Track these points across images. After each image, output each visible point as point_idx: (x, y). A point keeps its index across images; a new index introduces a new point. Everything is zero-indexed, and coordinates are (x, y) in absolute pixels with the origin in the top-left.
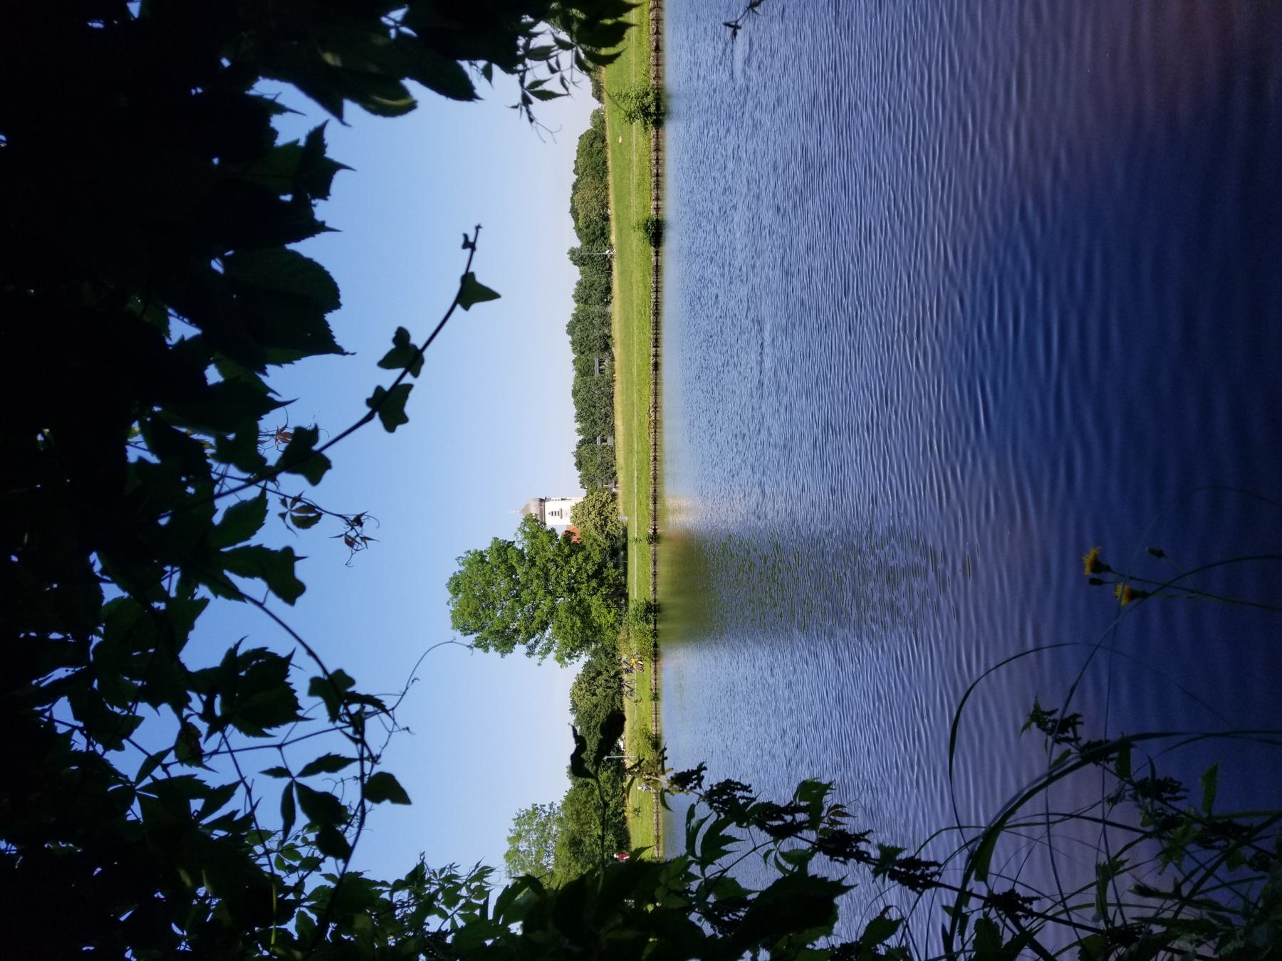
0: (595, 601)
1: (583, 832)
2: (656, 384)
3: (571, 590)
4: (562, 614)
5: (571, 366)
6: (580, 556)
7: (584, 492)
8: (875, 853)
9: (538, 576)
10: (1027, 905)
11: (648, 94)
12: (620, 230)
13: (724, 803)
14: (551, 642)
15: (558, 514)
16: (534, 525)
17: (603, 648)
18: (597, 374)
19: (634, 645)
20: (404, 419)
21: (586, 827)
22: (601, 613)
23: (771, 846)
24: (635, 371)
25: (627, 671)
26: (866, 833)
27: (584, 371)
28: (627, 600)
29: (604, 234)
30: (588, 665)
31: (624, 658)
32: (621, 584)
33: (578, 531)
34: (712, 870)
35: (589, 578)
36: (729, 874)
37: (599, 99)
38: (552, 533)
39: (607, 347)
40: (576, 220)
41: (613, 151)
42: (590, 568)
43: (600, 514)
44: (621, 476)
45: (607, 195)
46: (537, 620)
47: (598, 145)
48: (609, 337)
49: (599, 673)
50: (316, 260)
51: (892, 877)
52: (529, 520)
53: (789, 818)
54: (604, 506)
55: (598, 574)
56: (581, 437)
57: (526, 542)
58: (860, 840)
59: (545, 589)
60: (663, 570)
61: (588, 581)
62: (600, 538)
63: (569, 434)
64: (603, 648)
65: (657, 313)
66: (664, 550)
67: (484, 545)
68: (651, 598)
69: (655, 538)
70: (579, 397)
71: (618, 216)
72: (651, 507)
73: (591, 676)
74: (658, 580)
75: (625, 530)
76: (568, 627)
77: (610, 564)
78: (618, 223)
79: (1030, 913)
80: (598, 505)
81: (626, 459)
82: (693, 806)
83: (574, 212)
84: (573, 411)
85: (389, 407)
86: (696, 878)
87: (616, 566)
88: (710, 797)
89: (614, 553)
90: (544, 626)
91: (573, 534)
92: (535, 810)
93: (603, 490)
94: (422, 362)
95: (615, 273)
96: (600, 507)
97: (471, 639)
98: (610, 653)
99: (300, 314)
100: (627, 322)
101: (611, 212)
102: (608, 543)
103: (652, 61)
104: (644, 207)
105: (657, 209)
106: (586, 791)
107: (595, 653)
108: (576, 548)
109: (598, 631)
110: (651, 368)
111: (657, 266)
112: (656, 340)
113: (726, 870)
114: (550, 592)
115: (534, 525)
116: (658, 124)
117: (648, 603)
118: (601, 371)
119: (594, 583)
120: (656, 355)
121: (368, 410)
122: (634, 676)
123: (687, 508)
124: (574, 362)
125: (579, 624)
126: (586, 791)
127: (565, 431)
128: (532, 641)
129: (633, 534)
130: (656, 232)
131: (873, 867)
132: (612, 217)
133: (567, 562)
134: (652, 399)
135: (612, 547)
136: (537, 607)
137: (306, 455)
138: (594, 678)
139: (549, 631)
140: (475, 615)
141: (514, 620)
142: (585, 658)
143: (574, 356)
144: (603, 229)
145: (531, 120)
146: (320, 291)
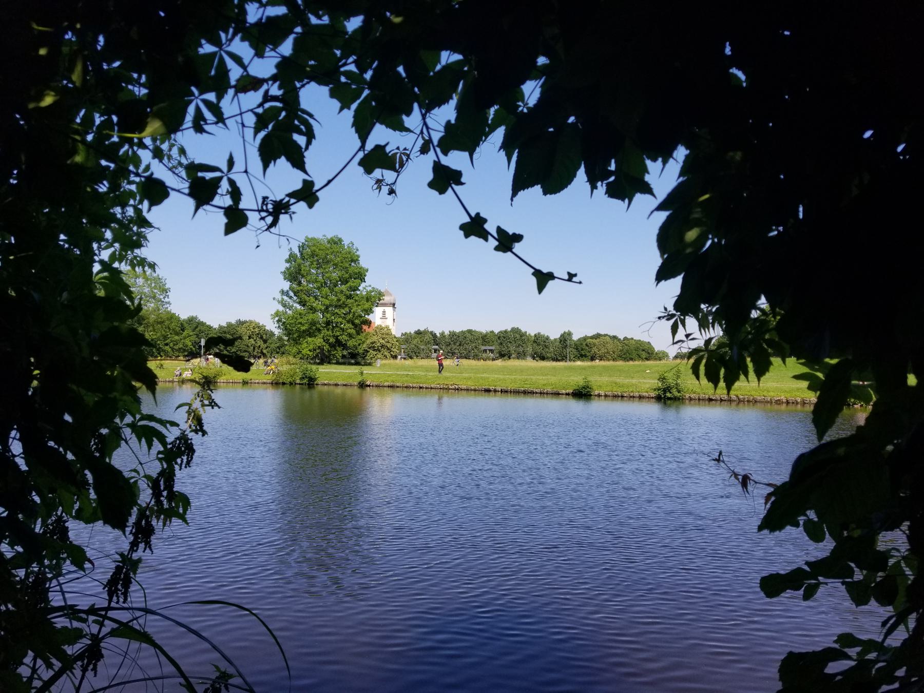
0: (318, 341)
1: (147, 326)
2: (475, 390)
3: (328, 323)
4: (311, 316)
5: (489, 329)
6: (353, 331)
7: (398, 335)
8: (135, 556)
9: (339, 300)
10: (91, 667)
11: (679, 392)
12: (584, 368)
13: (179, 448)
14: (290, 308)
15: (384, 316)
16: (374, 299)
17: (284, 345)
18: (483, 348)
19: (285, 368)
20: (467, 236)
21: (151, 328)
22: (309, 345)
23: (142, 474)
24: (485, 375)
25: (266, 362)
26: (151, 549)
27: (485, 338)
28: (319, 364)
29: (582, 356)
30: (272, 334)
31: (276, 361)
32: (330, 360)
33: (371, 330)
34: (127, 432)
35: (336, 337)
36: (123, 443)
37: (676, 357)
38: (369, 311)
39: (502, 356)
40: (592, 337)
41: (640, 366)
42: (344, 338)
43: (382, 346)
44: (409, 362)
45: (609, 360)
46: (307, 299)
47: (644, 355)
48: (509, 358)
49: (265, 341)
50: (575, 179)
51: (117, 567)
52: (380, 295)
53: (165, 494)
54: (388, 349)
55: (339, 343)
56: (438, 335)
57: (364, 293)
58: (146, 545)
59: (331, 311)
60: (339, 390)
61: (334, 336)
62: (364, 346)
63: (442, 326)
64: (284, 345)
65: (525, 393)
66: (356, 391)
67: (363, 263)
68: (319, 381)
69: (362, 385)
70: (468, 335)
71: (594, 367)
72: (386, 384)
73: (263, 335)
74: (332, 388)
75: (370, 364)
76: (300, 320)
77: (345, 353)
78: (589, 367)
79: (84, 670)
80: (389, 345)
81: (422, 367)
82: (178, 425)
83: (598, 336)
84: (458, 330)
85: (475, 227)
86: (122, 420)
87: (343, 357)
88: (183, 438)
89: (353, 356)
90: (303, 303)
91: (369, 326)
92: (165, 291)
93: (400, 349)
94: (505, 252)
95: (554, 364)
96: (387, 347)
97: (296, 251)
98: (280, 350)
99: (539, 170)
100: (521, 371)
101: (597, 362)
102: (361, 351)
103: (702, 396)
104: (600, 386)
105: (599, 396)
106: (178, 329)
107: (280, 339)
108: (359, 329)
109: (296, 342)
110: (486, 387)
111: (559, 394)
112: (507, 392)
113: (127, 442)
114: (327, 308)
115: (374, 299)
116: (658, 399)
117: (315, 379)
118: (485, 351)
119: (332, 340)
120: (495, 391)
121: (473, 215)
122: (262, 367)
123: (383, 409)
124: (492, 332)
125: (303, 328)
126: (178, 329)
127: (444, 324)
128: (292, 294)
129: (366, 370)
130: (582, 394)
131: (126, 553)
132: (593, 363)
133: (348, 322)
134: (464, 387)
135: (358, 354)
136: (316, 299)
137: (445, 179)
138: (262, 338)
139: (298, 307)
140: (313, 255)
141: (309, 282)
142: (277, 332)
143: (496, 332)
144: (585, 356)
145: (659, 318)
146: (554, 184)
